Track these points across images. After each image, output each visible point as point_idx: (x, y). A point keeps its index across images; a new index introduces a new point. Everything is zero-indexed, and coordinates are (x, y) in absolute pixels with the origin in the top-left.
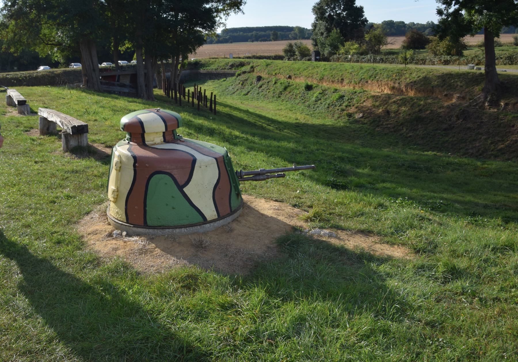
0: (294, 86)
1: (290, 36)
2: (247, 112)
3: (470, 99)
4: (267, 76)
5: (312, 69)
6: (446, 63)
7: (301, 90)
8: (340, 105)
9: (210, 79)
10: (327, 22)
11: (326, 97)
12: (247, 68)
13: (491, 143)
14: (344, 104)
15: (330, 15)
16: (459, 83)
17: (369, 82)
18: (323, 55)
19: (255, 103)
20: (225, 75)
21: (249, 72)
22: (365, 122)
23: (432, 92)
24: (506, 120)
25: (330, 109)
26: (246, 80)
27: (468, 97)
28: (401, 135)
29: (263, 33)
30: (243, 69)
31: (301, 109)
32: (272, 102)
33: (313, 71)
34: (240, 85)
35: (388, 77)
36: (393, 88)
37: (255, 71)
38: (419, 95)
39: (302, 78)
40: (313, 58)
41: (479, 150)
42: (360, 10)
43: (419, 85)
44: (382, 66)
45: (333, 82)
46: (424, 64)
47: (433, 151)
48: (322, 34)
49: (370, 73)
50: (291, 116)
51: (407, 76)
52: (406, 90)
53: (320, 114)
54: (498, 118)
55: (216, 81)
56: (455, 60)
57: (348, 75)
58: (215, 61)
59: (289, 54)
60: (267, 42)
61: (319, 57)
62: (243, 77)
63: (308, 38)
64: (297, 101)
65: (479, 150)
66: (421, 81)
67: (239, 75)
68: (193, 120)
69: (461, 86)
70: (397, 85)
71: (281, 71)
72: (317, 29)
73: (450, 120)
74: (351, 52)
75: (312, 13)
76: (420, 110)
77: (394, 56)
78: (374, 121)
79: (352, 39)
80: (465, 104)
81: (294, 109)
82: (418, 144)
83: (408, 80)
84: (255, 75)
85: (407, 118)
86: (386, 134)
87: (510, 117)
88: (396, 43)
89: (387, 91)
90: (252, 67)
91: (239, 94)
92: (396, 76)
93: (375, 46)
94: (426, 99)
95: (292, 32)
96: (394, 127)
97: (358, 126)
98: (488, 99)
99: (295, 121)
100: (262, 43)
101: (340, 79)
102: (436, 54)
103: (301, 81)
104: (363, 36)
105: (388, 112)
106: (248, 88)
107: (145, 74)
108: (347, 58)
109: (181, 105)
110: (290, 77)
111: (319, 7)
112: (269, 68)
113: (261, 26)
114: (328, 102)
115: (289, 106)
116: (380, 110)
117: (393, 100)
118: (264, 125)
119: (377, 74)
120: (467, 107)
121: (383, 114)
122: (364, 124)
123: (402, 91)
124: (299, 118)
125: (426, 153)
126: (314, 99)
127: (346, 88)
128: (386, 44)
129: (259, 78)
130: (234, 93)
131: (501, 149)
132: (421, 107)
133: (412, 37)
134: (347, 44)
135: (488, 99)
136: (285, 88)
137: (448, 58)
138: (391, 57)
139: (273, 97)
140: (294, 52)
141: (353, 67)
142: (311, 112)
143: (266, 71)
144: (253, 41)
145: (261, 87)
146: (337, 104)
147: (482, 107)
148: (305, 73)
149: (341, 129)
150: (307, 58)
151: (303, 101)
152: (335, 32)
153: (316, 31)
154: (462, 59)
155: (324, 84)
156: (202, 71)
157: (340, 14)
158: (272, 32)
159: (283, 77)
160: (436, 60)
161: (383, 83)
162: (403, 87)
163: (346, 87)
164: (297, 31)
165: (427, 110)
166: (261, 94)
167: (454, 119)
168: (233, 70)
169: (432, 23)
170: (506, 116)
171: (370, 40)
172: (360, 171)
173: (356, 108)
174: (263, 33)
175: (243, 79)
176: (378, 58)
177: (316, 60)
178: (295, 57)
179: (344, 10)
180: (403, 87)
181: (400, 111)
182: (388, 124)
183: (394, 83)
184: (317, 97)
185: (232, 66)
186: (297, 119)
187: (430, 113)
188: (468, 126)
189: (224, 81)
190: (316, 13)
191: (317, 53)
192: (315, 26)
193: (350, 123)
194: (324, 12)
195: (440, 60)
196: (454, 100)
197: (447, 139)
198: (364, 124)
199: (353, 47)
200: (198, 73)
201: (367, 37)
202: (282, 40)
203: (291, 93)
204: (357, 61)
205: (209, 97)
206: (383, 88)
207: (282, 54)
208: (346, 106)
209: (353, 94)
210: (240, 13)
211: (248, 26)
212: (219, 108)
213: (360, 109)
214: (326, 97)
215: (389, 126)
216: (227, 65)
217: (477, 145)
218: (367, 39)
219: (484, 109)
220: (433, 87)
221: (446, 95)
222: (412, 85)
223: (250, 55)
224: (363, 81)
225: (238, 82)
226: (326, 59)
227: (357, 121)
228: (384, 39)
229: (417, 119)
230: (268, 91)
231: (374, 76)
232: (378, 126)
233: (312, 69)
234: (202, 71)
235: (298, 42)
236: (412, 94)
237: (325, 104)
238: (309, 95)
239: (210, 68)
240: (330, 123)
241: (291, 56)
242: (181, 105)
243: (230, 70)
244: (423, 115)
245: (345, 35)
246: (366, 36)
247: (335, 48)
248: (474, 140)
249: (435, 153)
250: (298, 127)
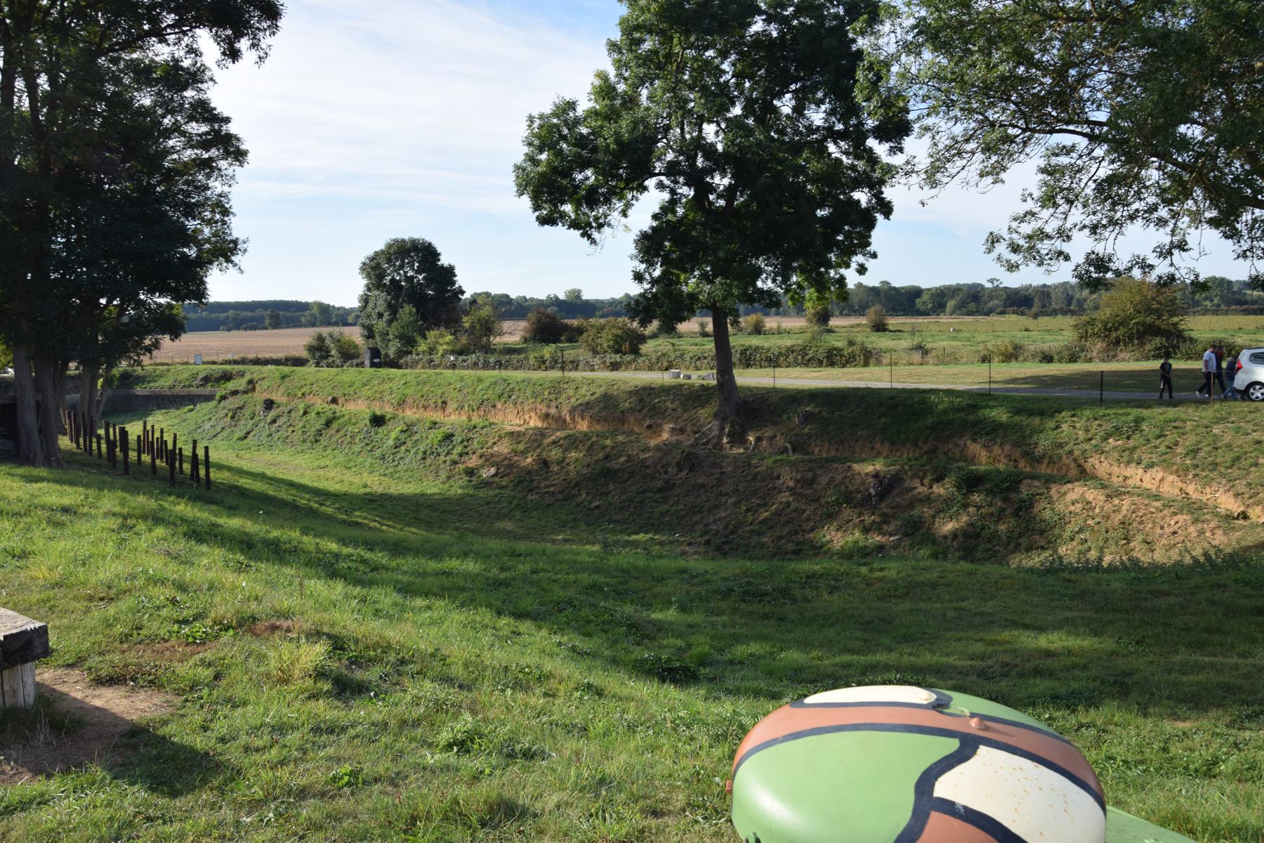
0: (346, 418)
1: (303, 319)
2: (263, 477)
3: (696, 433)
4: (284, 400)
5: (380, 384)
6: (615, 366)
7: (361, 425)
8: (448, 453)
9: (159, 408)
10: (389, 294)
11: (415, 438)
12: (240, 384)
13: (748, 511)
14: (455, 452)
15: (393, 280)
16: (668, 404)
17: (499, 406)
18: (387, 355)
19: (267, 456)
20: (193, 400)
21: (245, 392)
22: (504, 483)
23: (622, 420)
24: (764, 468)
25: (429, 461)
26: (240, 408)
27: (689, 428)
28: (578, 505)
29: (249, 314)
30: (231, 385)
31: (367, 464)
32: (303, 451)
33: (381, 388)
34: (228, 419)
35: (535, 395)
36: (547, 416)
37: (258, 389)
38: (598, 428)
39: (360, 402)
40: (367, 362)
41: (727, 526)
42: (449, 272)
43: (596, 410)
44: (519, 375)
45: (425, 408)
46: (576, 369)
47: (646, 532)
48: (380, 315)
49: (499, 390)
50: (351, 479)
51: (571, 392)
52: (573, 419)
53: (409, 473)
54: (749, 465)
55: (173, 412)
56: (630, 363)
57: (455, 394)
58: (168, 371)
59: (317, 354)
60: (258, 332)
61: (379, 359)
62: (233, 402)
63: (354, 324)
64: (356, 449)
65: (727, 526)
66: (598, 401)
67: (224, 398)
68: (221, 521)
69: (674, 410)
70: (553, 411)
71: (315, 388)
72: (370, 305)
73: (666, 473)
74: (441, 349)
75: (360, 277)
76: (607, 457)
77: (522, 356)
78: (521, 482)
79: (437, 325)
80: (687, 441)
81: (352, 464)
82: (616, 521)
83: (573, 400)
84: (259, 396)
85: (585, 471)
86: (549, 505)
87: (769, 462)
88: (512, 333)
89: (535, 423)
90: (251, 382)
91: (228, 438)
92: (550, 393)
93: (480, 338)
94: (614, 433)
95: (307, 312)
96: (562, 492)
97: (491, 493)
98: (727, 430)
99: (362, 491)
100: (249, 332)
101: (439, 401)
102: (595, 352)
103: (360, 409)
104: (458, 320)
105: (545, 463)
106: (245, 424)
107: (37, 403)
108: (431, 361)
109: (127, 472)
110: (334, 401)
111: (373, 264)
112: (287, 382)
113: (244, 300)
114: (422, 447)
115: (341, 458)
116: (529, 460)
117: (550, 439)
118: (312, 504)
119: (512, 390)
120: (691, 446)
121: (536, 467)
122: (502, 488)
123: (565, 421)
124: (369, 483)
125: (634, 537)
126: (391, 442)
127: (453, 419)
128: (501, 334)
129: (269, 404)
130: (215, 436)
131: (765, 521)
132: (608, 450)
133: (539, 321)
134: (432, 334)
135: (727, 430)
136: (328, 424)
137: (617, 358)
138: (515, 357)
139: (304, 441)
140: (328, 351)
141: (462, 379)
142: (391, 470)
143: (282, 389)
144: (229, 330)
145: (274, 421)
146: (440, 450)
147: (719, 446)
148: (366, 391)
149: (460, 500)
150: (355, 361)
151: (369, 448)
152: (407, 311)
153: (369, 309)
154: (640, 360)
155: (408, 413)
156: (139, 390)
157: (412, 278)
158: (269, 312)
159: (319, 401)
160: (596, 361)
161: (526, 408)
162: (565, 413)
163: (452, 417)
164: (315, 311)
165: (620, 456)
166: (276, 437)
167: (672, 470)
168: (208, 389)
169: (557, 298)
170: (763, 459)
171: (473, 327)
172: (656, 616)
173: (481, 457)
174: (249, 314)
175: (232, 406)
176: (492, 360)
177: (373, 365)
178: (331, 359)
179: (419, 272)
180: (565, 413)
181: (567, 461)
182: (549, 486)
183: (549, 407)
184: (397, 439)
185: (206, 380)
186: (365, 486)
187: (627, 461)
188: (700, 481)
189: (191, 411)
190: (369, 276)
191: (375, 353)
192: (365, 300)
193: (476, 488)
194: (381, 277)
195: (604, 363)
196: (665, 436)
197: (666, 507)
198: (502, 488)
199: (441, 339)
200: (132, 400)
201: (466, 322)
202: (288, 327)
203: (342, 433)
204: (453, 366)
205: (187, 452)
206: (527, 417)
207: (304, 354)
208: (460, 455)
209: (470, 430)
210: (232, 271)
211: (300, 300)
212: (215, 475)
213: (488, 460)
214: (415, 438)
215: (552, 489)
216: (196, 378)
217: (723, 515)
218: (467, 325)
219: (722, 448)
220: (622, 412)
221: (649, 427)
222: (583, 409)
223: (236, 357)
224: (485, 405)
225: (222, 413)
226: (394, 364)
227: (486, 484)
228: (496, 325)
229: (604, 475)
230: (291, 429)
231: (507, 394)
232: (531, 491)
233: (380, 384)
234: (139, 390)
235: (336, 330)
236: (583, 426)
237: (416, 453)
238: (380, 436)
239: (156, 384)
240: (435, 490)
241: (323, 358)
242: (127, 472)
243: (201, 389)
244: (613, 465)
245: (424, 318)
246: (465, 319)
247: (408, 342)
248: (716, 507)
249: (650, 535)
250: (373, 502)
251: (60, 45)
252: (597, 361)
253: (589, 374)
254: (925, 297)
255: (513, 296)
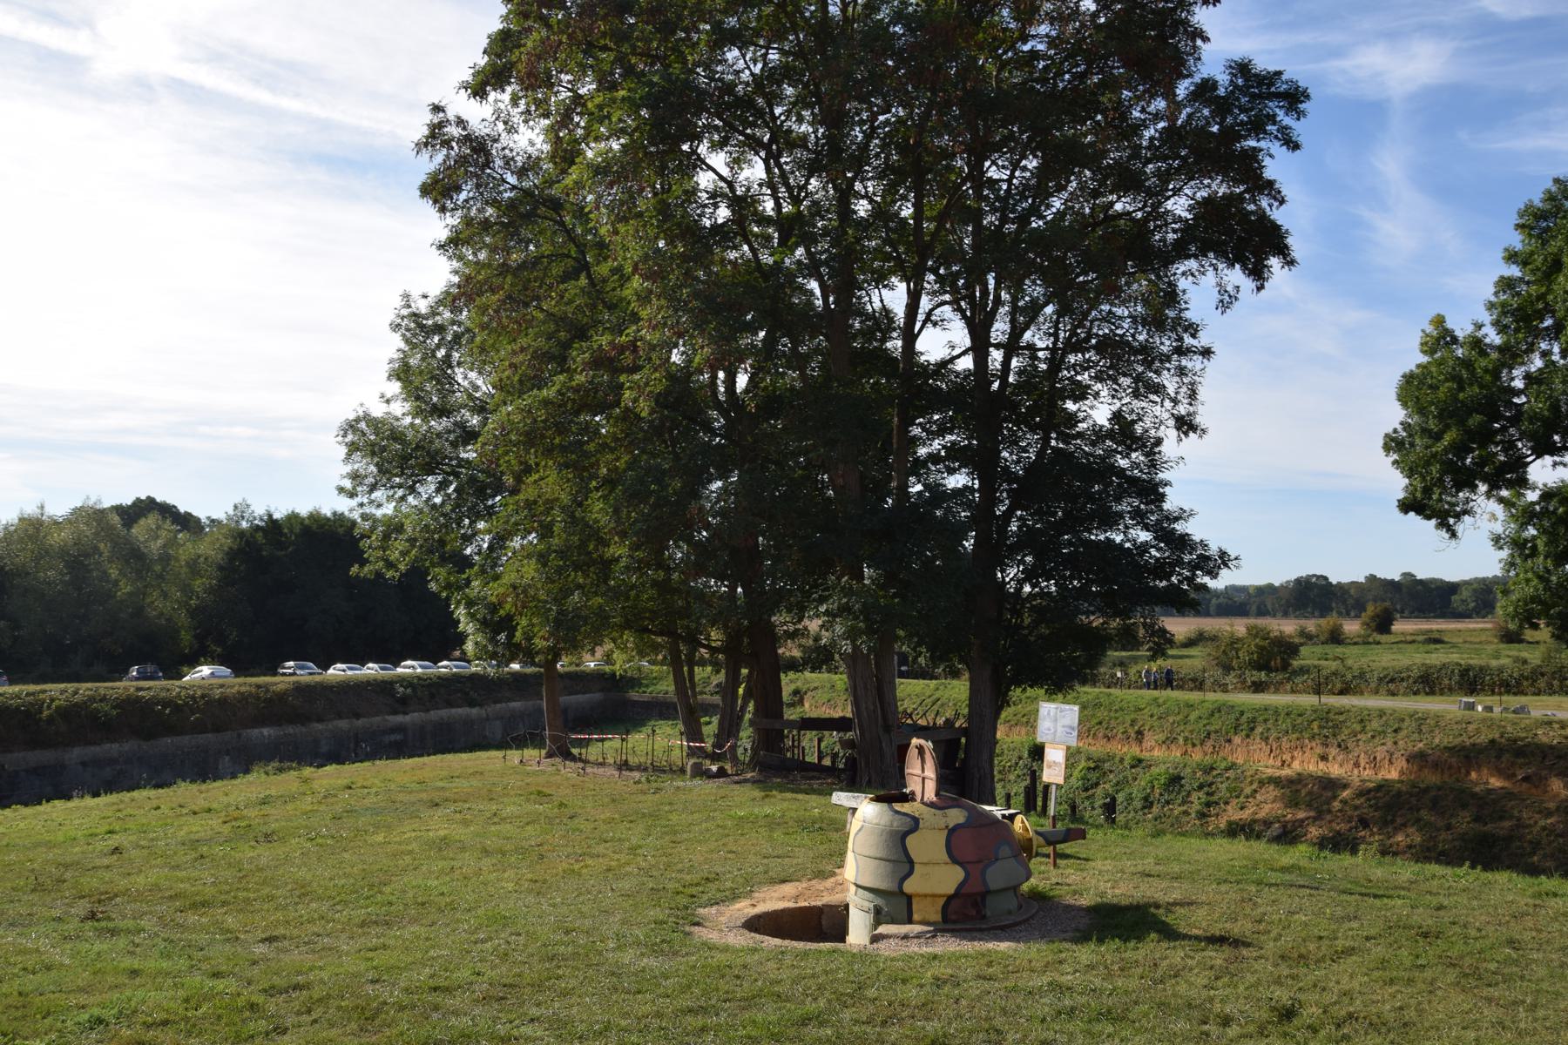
6: (1258, 687)
17: (1237, 740)
92: (1320, 727)
234: (634, 695)
251: (611, 208)
252: (1231, 679)
253: (1219, 697)
254: (1465, 594)
255: (1277, 584)
